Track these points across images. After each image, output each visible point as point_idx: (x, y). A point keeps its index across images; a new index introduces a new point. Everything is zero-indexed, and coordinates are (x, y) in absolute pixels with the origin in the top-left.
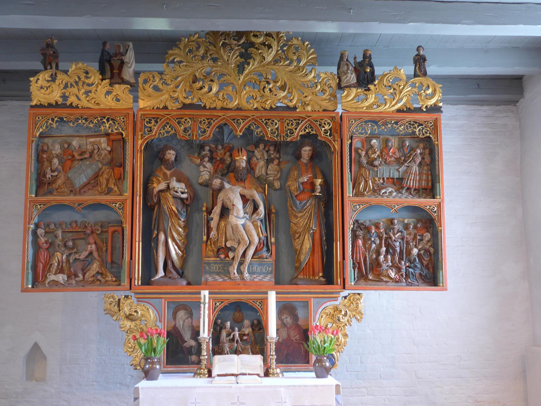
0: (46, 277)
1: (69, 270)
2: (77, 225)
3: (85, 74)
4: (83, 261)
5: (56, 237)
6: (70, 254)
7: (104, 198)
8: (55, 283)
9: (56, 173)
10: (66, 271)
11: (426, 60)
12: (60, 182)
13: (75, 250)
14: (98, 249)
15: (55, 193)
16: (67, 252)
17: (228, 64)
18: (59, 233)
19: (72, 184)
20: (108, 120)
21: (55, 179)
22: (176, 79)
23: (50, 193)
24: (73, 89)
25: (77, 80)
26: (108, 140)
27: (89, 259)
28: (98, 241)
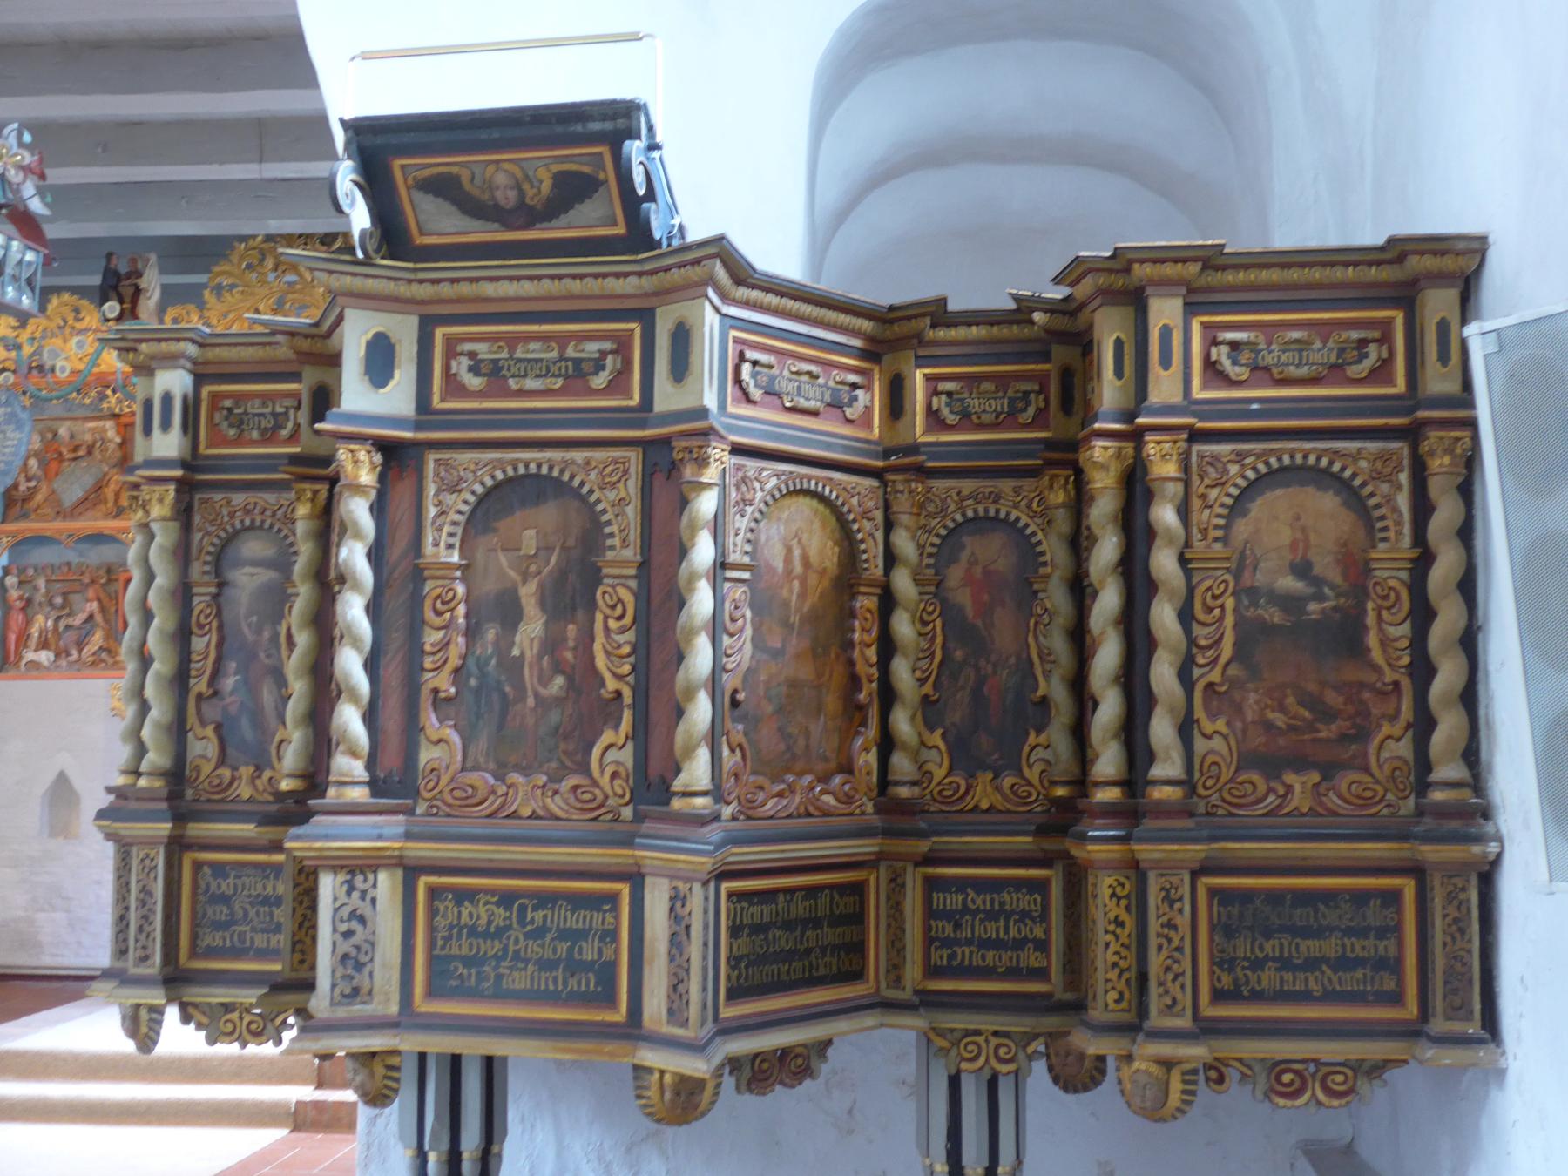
0: (21, 658)
1: (57, 645)
2: (70, 569)
3: (73, 314)
4: (79, 628)
5: (36, 589)
6: (58, 619)
7: (108, 525)
8: (34, 665)
9: (33, 484)
10: (53, 647)
11: (942, 301)
12: (39, 498)
13: (67, 611)
14: (103, 610)
15: (33, 517)
16: (54, 614)
17: (314, 287)
18: (41, 583)
19: (59, 502)
20: (114, 391)
21: (32, 492)
22: (225, 317)
23: (24, 516)
24: (54, 340)
25: (62, 324)
26: (118, 425)
27: (88, 626)
28: (102, 596)
